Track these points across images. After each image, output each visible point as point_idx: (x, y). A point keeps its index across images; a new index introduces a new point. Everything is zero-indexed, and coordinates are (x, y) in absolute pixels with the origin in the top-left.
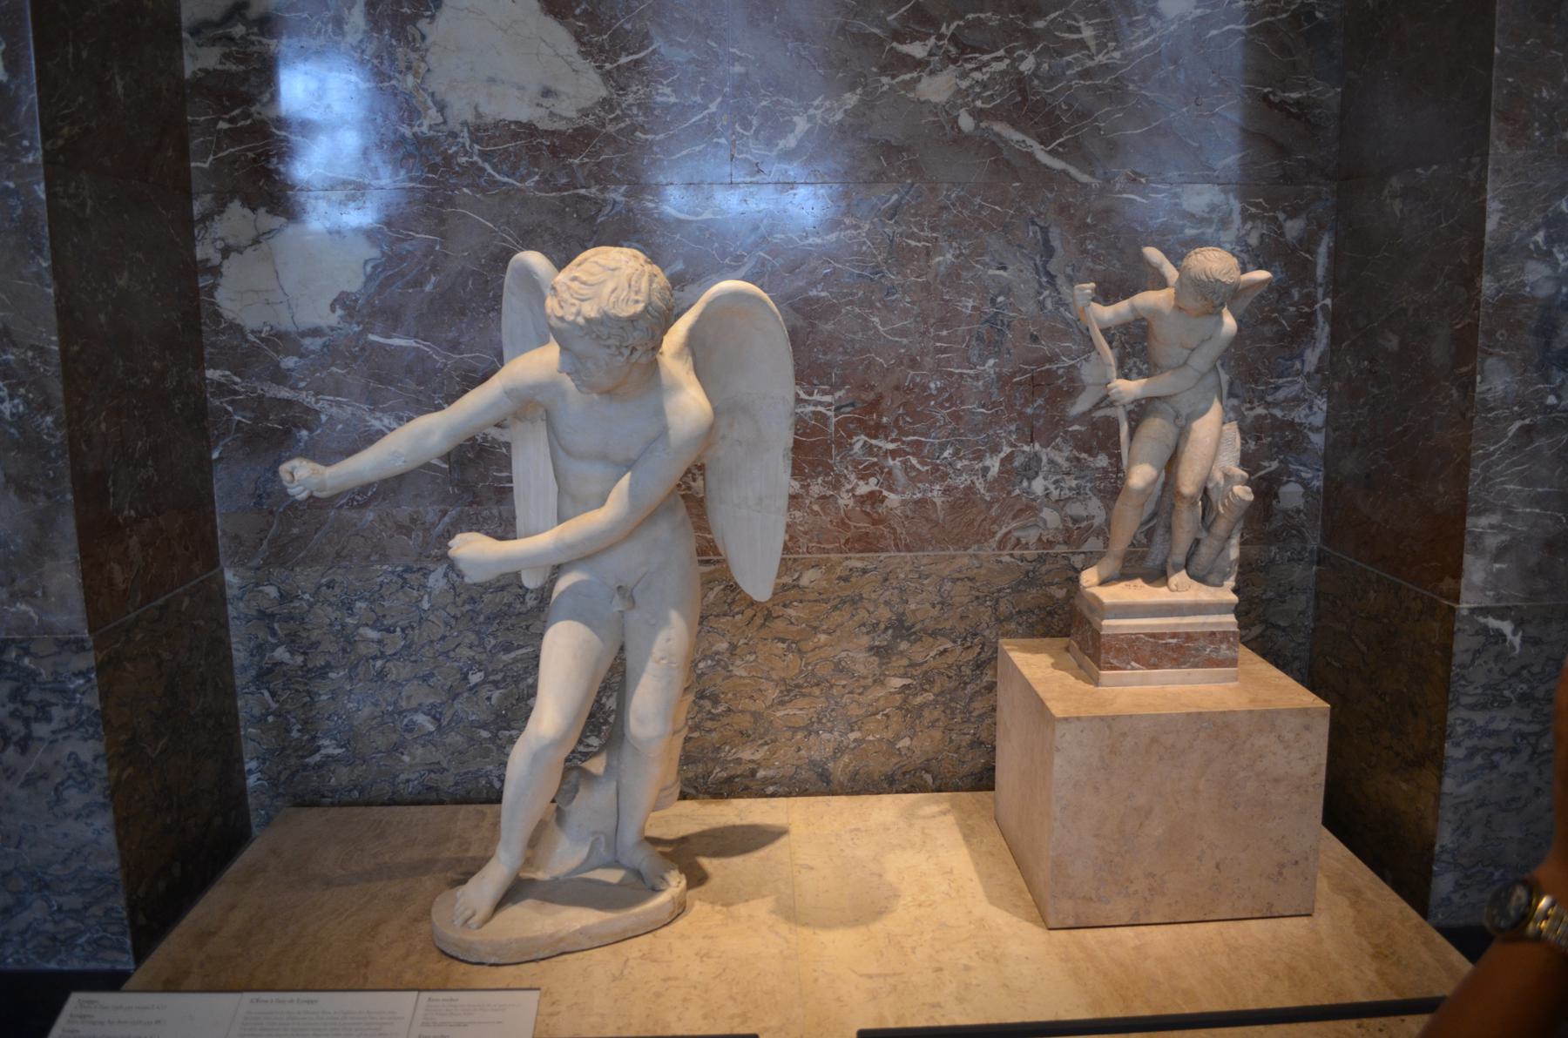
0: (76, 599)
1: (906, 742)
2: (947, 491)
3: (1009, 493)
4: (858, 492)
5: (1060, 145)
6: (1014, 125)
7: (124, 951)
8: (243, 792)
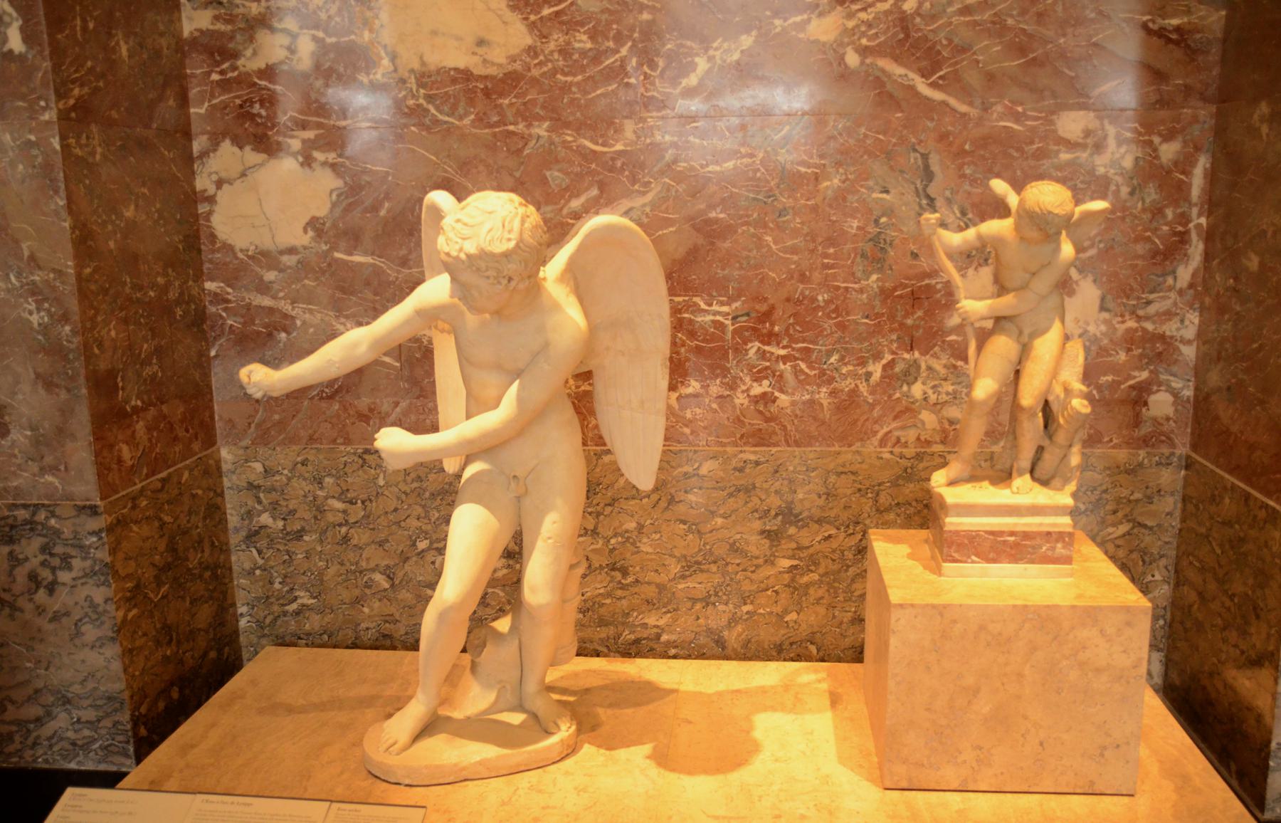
0: (90, 474)
1: (793, 616)
2: (833, 393)
3: (890, 396)
4: (753, 393)
5: (940, 78)
6: (897, 59)
7: (127, 756)
8: (236, 632)
